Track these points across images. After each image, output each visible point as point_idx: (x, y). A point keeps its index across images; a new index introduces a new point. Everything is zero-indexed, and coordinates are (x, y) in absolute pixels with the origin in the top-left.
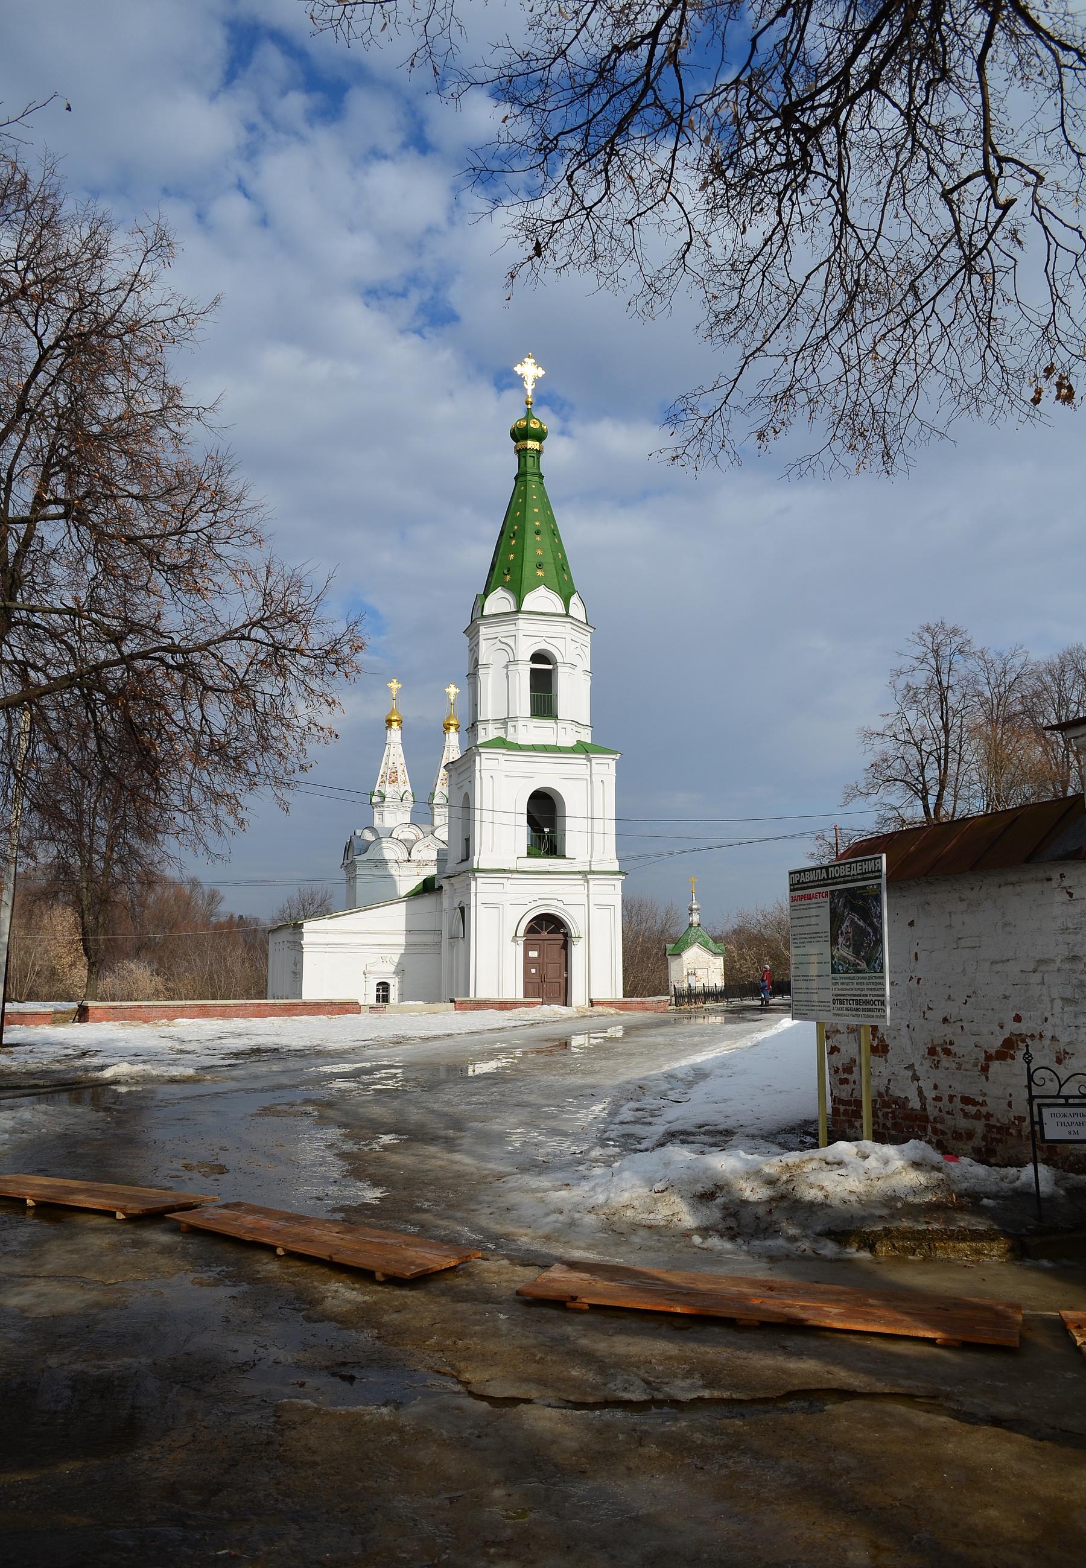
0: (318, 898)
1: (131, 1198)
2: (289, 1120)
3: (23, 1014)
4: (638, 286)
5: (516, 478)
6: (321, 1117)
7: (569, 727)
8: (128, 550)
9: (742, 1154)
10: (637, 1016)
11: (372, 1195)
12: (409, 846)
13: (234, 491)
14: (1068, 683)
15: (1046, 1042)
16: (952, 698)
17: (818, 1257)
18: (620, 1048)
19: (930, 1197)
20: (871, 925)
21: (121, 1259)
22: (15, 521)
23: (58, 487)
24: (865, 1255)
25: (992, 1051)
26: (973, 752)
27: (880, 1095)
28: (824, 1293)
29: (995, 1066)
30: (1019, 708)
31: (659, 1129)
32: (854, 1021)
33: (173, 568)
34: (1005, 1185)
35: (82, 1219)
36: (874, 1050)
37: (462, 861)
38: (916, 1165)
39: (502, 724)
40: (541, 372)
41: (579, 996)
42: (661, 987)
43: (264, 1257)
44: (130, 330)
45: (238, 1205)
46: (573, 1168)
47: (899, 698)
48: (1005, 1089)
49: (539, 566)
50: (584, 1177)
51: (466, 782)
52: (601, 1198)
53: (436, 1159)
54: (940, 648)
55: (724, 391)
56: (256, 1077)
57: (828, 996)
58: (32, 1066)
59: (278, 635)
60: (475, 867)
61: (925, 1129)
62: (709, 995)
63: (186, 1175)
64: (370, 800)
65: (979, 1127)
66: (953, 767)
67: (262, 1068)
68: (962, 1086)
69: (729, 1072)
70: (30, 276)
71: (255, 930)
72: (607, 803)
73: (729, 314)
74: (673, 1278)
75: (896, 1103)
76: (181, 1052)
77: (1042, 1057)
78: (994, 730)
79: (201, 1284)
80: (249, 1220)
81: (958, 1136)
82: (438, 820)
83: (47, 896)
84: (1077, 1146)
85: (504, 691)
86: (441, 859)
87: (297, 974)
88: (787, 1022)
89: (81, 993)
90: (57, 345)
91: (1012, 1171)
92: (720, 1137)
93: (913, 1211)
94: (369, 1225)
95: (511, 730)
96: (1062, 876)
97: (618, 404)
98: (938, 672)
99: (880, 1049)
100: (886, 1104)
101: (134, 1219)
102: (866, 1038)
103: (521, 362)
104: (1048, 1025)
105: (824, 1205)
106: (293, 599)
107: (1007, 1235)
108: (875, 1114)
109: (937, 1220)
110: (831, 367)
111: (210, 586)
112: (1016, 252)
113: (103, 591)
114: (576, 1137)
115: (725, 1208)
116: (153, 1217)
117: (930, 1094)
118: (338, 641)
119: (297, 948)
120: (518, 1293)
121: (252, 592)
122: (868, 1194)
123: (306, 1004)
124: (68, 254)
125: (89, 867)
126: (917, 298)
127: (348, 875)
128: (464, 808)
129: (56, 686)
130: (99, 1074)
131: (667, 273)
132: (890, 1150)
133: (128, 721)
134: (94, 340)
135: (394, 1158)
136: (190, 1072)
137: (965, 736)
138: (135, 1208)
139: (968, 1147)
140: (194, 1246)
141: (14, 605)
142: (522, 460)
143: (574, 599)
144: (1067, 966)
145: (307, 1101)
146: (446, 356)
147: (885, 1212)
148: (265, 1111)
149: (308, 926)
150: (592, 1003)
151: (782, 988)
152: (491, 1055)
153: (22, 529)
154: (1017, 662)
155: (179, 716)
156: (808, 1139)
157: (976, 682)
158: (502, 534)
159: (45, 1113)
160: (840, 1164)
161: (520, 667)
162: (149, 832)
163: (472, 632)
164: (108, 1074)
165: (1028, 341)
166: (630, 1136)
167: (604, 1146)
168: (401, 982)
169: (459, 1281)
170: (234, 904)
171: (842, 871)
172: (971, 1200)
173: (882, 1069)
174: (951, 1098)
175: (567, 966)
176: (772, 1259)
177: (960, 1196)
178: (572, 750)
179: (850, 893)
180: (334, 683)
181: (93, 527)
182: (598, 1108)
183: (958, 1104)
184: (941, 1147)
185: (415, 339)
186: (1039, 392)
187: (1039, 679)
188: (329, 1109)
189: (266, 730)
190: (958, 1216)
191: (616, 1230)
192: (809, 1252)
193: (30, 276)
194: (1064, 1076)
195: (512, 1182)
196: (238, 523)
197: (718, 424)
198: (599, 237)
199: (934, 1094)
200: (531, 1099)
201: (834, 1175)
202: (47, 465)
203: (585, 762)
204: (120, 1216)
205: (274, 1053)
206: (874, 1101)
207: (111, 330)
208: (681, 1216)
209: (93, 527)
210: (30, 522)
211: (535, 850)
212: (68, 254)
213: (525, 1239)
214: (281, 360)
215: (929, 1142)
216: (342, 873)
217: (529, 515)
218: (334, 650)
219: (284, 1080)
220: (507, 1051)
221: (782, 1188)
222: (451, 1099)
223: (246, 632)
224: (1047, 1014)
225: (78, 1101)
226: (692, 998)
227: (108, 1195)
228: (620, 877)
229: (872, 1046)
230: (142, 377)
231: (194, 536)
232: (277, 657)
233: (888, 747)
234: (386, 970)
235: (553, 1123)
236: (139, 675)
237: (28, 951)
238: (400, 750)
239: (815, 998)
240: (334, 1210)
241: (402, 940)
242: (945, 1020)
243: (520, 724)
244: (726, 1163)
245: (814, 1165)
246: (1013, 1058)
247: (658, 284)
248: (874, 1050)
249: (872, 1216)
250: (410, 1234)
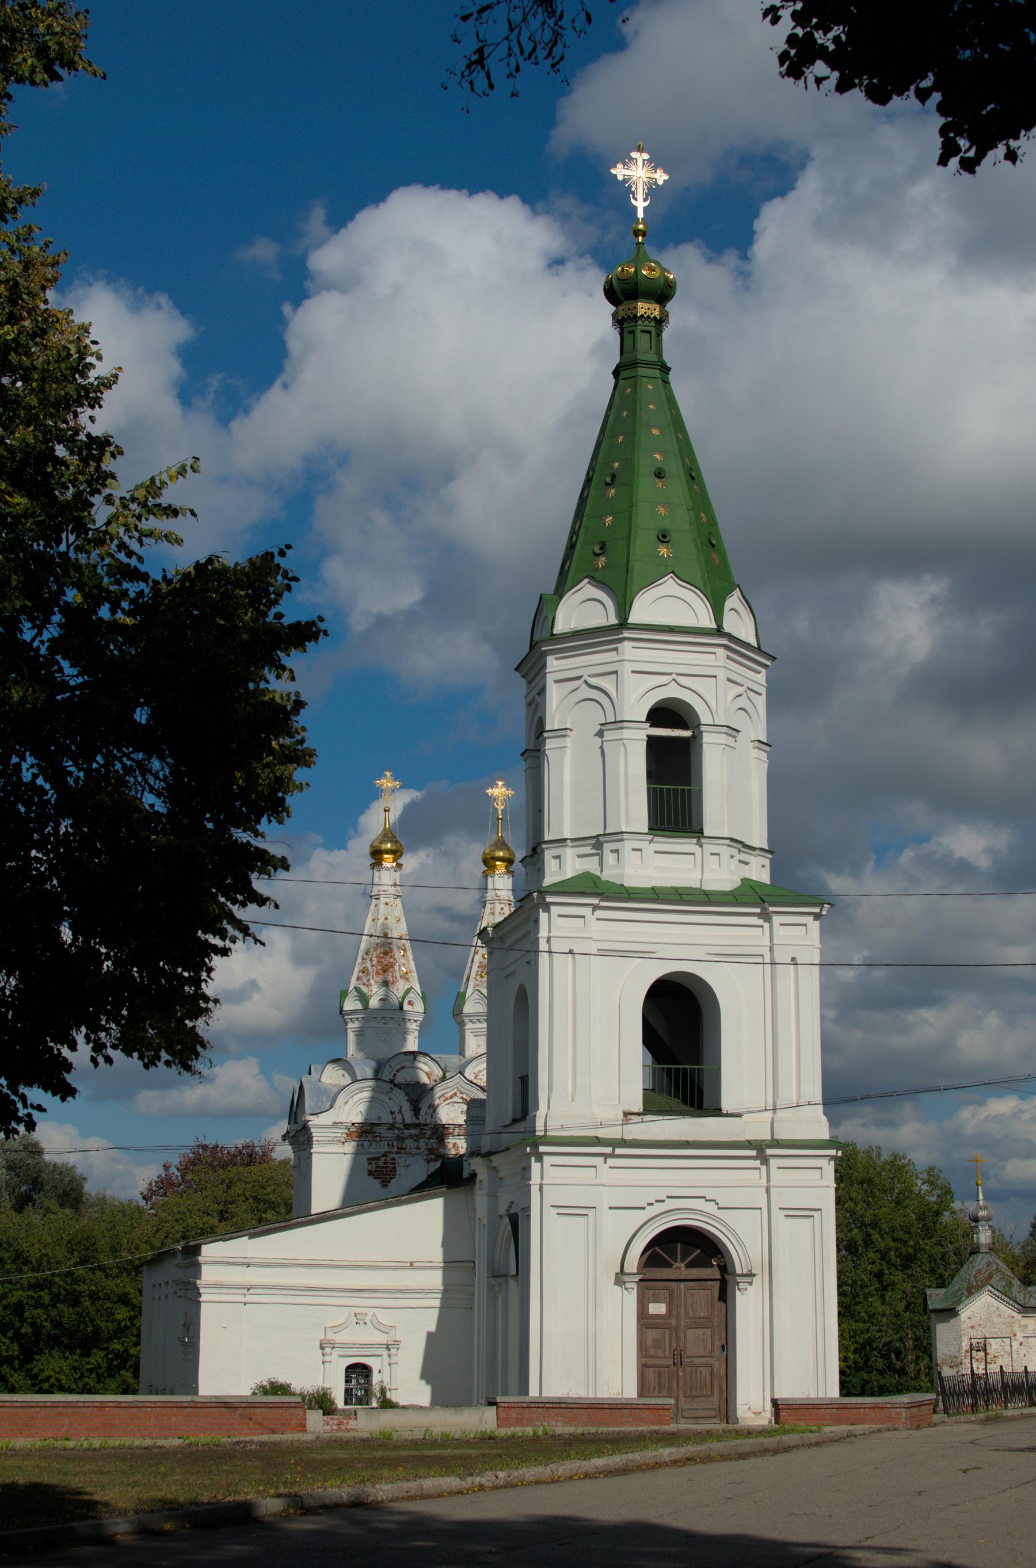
5: (616, 373)
7: (725, 851)
37: (515, 1121)
39: (594, 847)
49: (663, 538)
60: (540, 1133)
72: (803, 998)
95: (610, 858)
103: (627, 161)
119: (189, 1295)
142: (628, 338)
143: (734, 601)
149: (210, 1251)
158: (589, 480)
161: (626, 734)
163: (531, 668)
203: (760, 922)
211: (663, 1099)
228: (833, 1152)
241: (435, 1279)
243: (628, 845)
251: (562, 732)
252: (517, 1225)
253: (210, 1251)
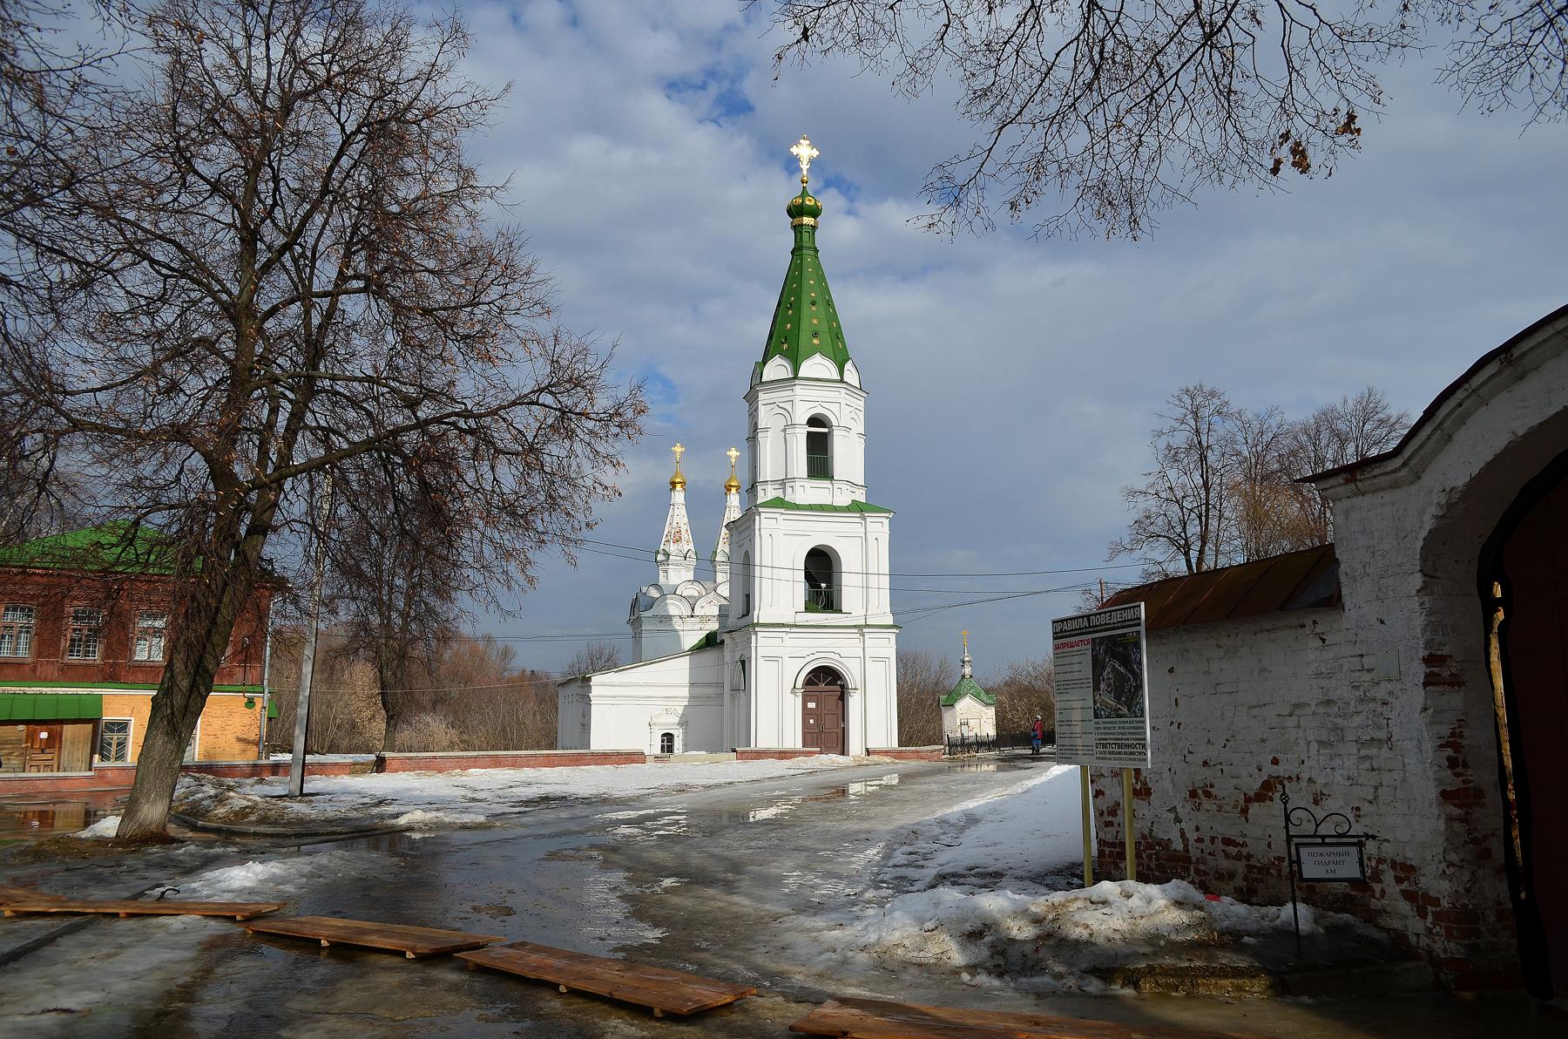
0: (606, 653)
1: (420, 938)
3: (324, 765)
4: (902, 66)
6: (606, 861)
7: (844, 487)
8: (432, 323)
9: (1009, 893)
10: (913, 764)
11: (652, 935)
12: (692, 602)
13: (523, 264)
14: (1324, 442)
15: (1304, 784)
16: (1212, 458)
17: (1084, 994)
18: (895, 795)
20: (1132, 671)
21: (410, 996)
22: (318, 295)
23: (360, 262)
24: (1129, 992)
25: (1251, 794)
26: (1232, 509)
27: (1144, 837)
28: (1089, 1028)
29: (1255, 808)
31: (930, 872)
32: (1116, 765)
33: (465, 337)
34: (1265, 923)
35: (373, 958)
36: (1136, 793)
38: (1179, 904)
40: (815, 153)
41: (855, 746)
42: (936, 738)
43: (547, 995)
44: (427, 116)
45: (523, 944)
46: (847, 908)
48: (1264, 829)
49: (815, 335)
50: (858, 918)
52: (873, 938)
53: (715, 900)
54: (1198, 407)
55: (977, 162)
56: (544, 824)
57: (1091, 740)
58: (330, 814)
59: (567, 401)
61: (1188, 870)
62: (982, 744)
63: (475, 916)
64: (655, 559)
65: (1240, 867)
66: (1213, 524)
67: (549, 815)
69: (1000, 817)
70: (336, 68)
71: (547, 685)
73: (985, 93)
74: (942, 1014)
75: (1159, 844)
76: (474, 800)
77: (1299, 797)
79: (487, 1021)
80: (534, 959)
81: (1220, 876)
82: (720, 577)
83: (348, 652)
84: (1335, 884)
85: (783, 453)
86: (723, 615)
87: (585, 726)
88: (1057, 770)
89: (379, 745)
90: (358, 131)
91: (1273, 910)
92: (990, 878)
93: (1176, 948)
94: (649, 964)
95: (789, 490)
96: (1315, 622)
98: (1197, 432)
99: (1143, 792)
100: (1150, 846)
101: (425, 959)
102: (1129, 780)
103: (797, 143)
105: (1089, 943)
106: (580, 366)
107: (1268, 972)
108: (1138, 855)
109: (1199, 958)
110: (1078, 139)
111: (501, 354)
112: (1255, 31)
114: (851, 880)
115: (993, 946)
116: (441, 956)
117: (1192, 836)
118: (621, 405)
119: (586, 700)
120: (791, 1028)
122: (1132, 932)
123: (593, 754)
124: (371, 48)
125: (387, 625)
126: (1161, 74)
127: (635, 630)
128: (745, 566)
129: (355, 450)
131: (927, 53)
132: (1153, 890)
133: (424, 484)
134: (394, 125)
135: (675, 900)
136: (482, 819)
137: (1225, 493)
138: (424, 948)
139: (1230, 887)
140: (479, 984)
143: (849, 366)
144: (1322, 710)
145: (593, 847)
146: (741, 143)
147: (1148, 950)
148: (553, 856)
149: (596, 679)
150: (868, 752)
151: (1049, 738)
152: (770, 802)
153: (325, 303)
154: (1273, 422)
155: (470, 476)
157: (1234, 442)
159: (341, 858)
160: (1105, 903)
162: (443, 591)
163: (751, 398)
164: (403, 821)
165: (1266, 114)
166: (902, 878)
167: (877, 888)
168: (685, 733)
169: (734, 1017)
170: (528, 659)
171: (1103, 619)
172: (1232, 938)
174: (1213, 839)
175: (844, 716)
176: (1039, 996)
177: (1221, 934)
178: (848, 509)
179: (1109, 645)
181: (392, 300)
182: (872, 852)
183: (1219, 845)
184: (1203, 887)
185: (712, 128)
186: (1278, 162)
187: (1295, 438)
188: (613, 854)
189: (556, 492)
191: (887, 967)
192: (1074, 989)
194: (1319, 817)
195: (788, 922)
196: (527, 295)
197: (973, 193)
198: (862, 22)
199: (1195, 835)
200: (808, 843)
201: (1098, 914)
202: (349, 245)
204: (410, 955)
205: (563, 800)
206: (1138, 844)
207: (409, 116)
208: (950, 954)
209: (392, 300)
210: (333, 295)
211: (813, 606)
212: (371, 48)
213: (799, 977)
214: (586, 148)
215: (1192, 882)
216: (629, 629)
218: (617, 414)
220: (786, 798)
221: (1048, 927)
222: (731, 844)
223: (534, 398)
224: (1304, 757)
225: (376, 848)
226: (966, 746)
227: (399, 935)
229: (1135, 790)
230: (439, 160)
231: (486, 307)
233: (1151, 504)
234: (670, 721)
235: (829, 867)
236: (434, 439)
237: (329, 706)
238: (683, 511)
239: (1079, 742)
240: (616, 950)
241: (685, 692)
242: (1205, 763)
243: (798, 484)
244: (993, 903)
245: (1079, 904)
246: (1271, 799)
247: (919, 64)
248: (1136, 793)
249: (1136, 954)
250: (688, 972)
251: (766, 429)
252: (744, 664)
253: (596, 679)
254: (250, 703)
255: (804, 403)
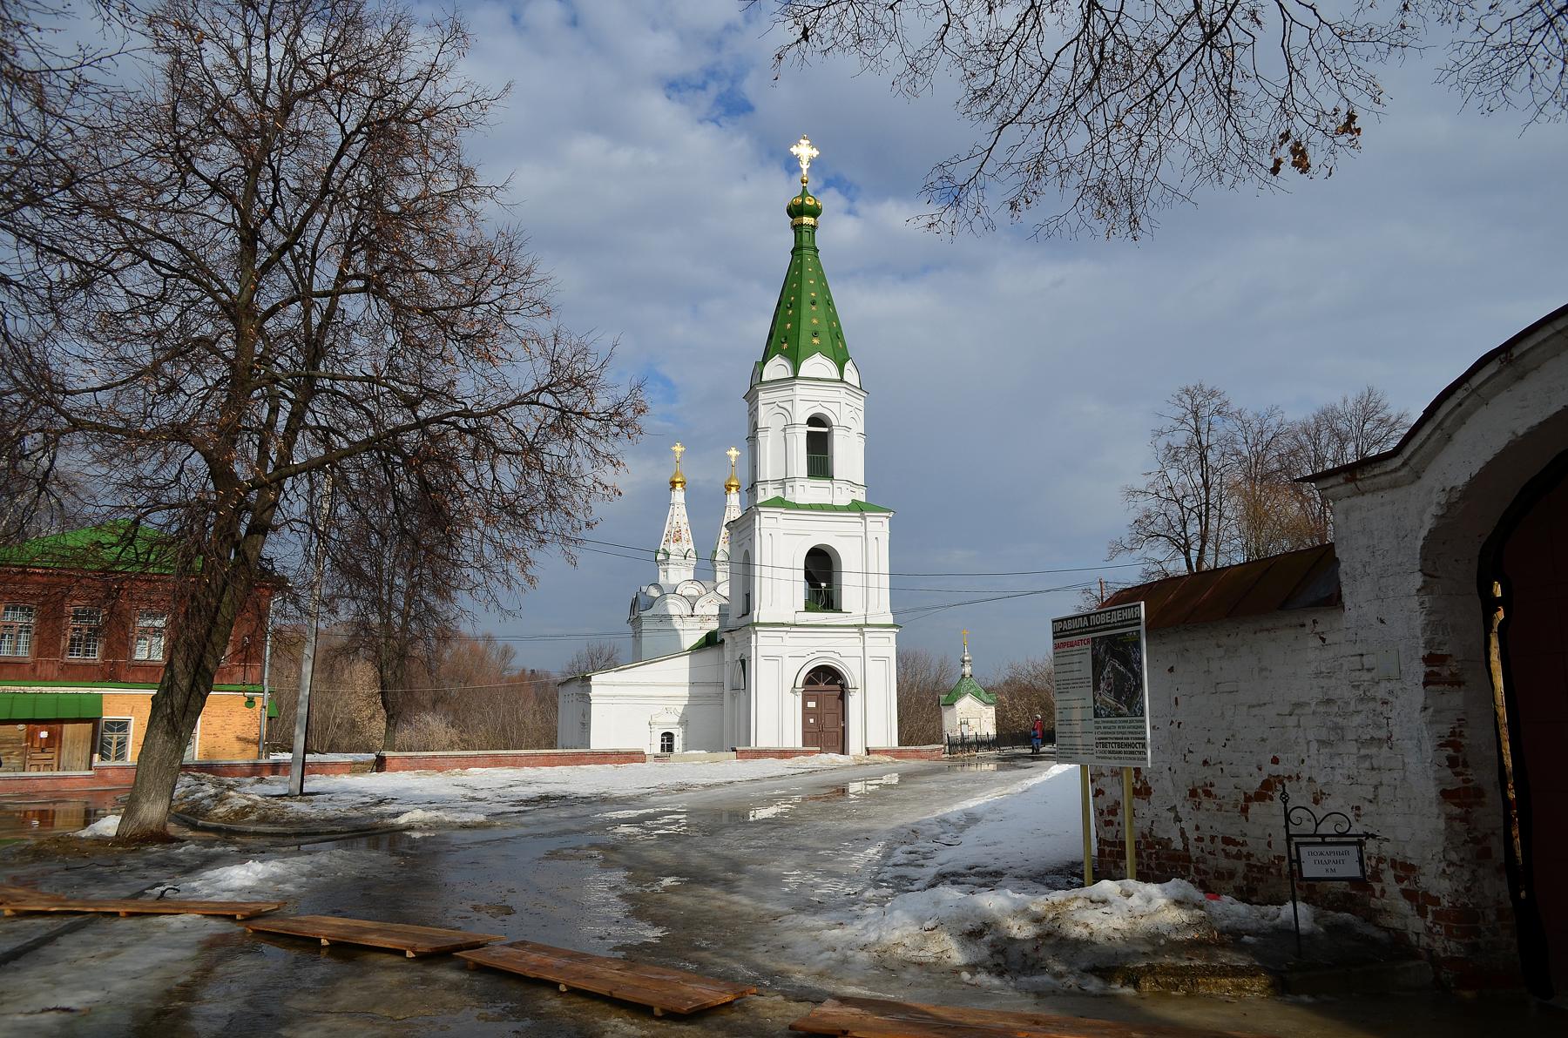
0: (606, 652)
1: (420, 937)
2: (573, 863)
3: (324, 764)
4: (902, 66)
6: (606, 860)
7: (844, 487)
8: (431, 323)
9: (1009, 892)
10: (913, 764)
11: (652, 934)
12: (692, 602)
14: (1324, 442)
15: (1304, 783)
16: (1212, 457)
17: (1084, 993)
18: (895, 794)
19: (1192, 935)
20: (1132, 670)
21: (410, 995)
22: (318, 295)
23: (360, 261)
24: (1129, 991)
26: (1232, 508)
27: (1144, 836)
28: (1089, 1027)
29: (1255, 807)
30: (1276, 466)
31: (931, 871)
32: (1116, 764)
33: (465, 337)
34: (1265, 923)
35: (373, 957)
36: (1136, 792)
38: (1179, 903)
40: (815, 153)
41: (855, 745)
42: (936, 738)
43: (547, 994)
44: (427, 116)
45: (523, 943)
46: (847, 907)
47: (1161, 457)
48: (1264, 828)
49: (815, 334)
50: (858, 917)
51: (746, 541)
52: (873, 937)
53: (715, 899)
54: (1199, 407)
55: (978, 161)
56: (544, 823)
57: (1091, 739)
61: (1188, 869)
62: (981, 743)
63: (475, 916)
64: (655, 558)
65: (1240, 866)
66: (1213, 523)
67: (549, 814)
68: (1222, 827)
69: (1000, 816)
70: (336, 68)
71: (547, 684)
72: (881, 560)
73: (985, 92)
75: (1159, 843)
76: (474, 799)
77: (1299, 796)
78: (1253, 488)
80: (534, 958)
81: (1220, 875)
82: (720, 577)
83: (348, 651)
85: (783, 453)
86: (723, 615)
87: (585, 725)
88: (1057, 769)
89: (379, 744)
90: (358, 130)
91: (1273, 909)
92: (990, 878)
93: (1177, 947)
94: (649, 963)
95: (789, 490)
97: (893, 185)
98: (1198, 432)
99: (1143, 792)
100: (1150, 846)
101: (425, 958)
102: (1129, 780)
103: (797, 143)
104: (1304, 767)
105: (1089, 943)
106: (580, 365)
107: (1268, 971)
108: (1138, 854)
109: (1199, 957)
110: (1078, 139)
111: (501, 354)
112: (1255, 31)
113: (401, 361)
114: (851, 879)
115: (993, 945)
116: (441, 955)
117: (1192, 835)
118: (621, 405)
119: (586, 700)
120: (791, 1027)
121: (542, 359)
122: (1132, 931)
123: (593, 754)
124: (371, 48)
125: (387, 624)
126: (1161, 74)
127: (636, 629)
128: (745, 565)
129: (354, 450)
130: (394, 821)
131: (927, 53)
132: (1153, 889)
134: (394, 125)
135: (675, 899)
136: (482, 818)
137: (1225, 493)
138: (424, 947)
139: (1230, 886)
140: (479, 983)
141: (316, 373)
143: (849, 365)
144: (1322, 709)
145: (593, 846)
146: (741, 143)
147: (1148, 949)
148: (553, 855)
149: (596, 679)
150: (868, 751)
151: (1049, 737)
152: (770, 801)
153: (325, 302)
154: (1273, 422)
155: (470, 476)
156: (1076, 880)
157: (1234, 441)
159: (341, 858)
160: (1105, 902)
162: (443, 590)
163: (751, 397)
164: (402, 820)
165: (1266, 114)
166: (902, 877)
167: (877, 887)
168: (685, 733)
169: (734, 1016)
170: (527, 658)
171: (1103, 619)
172: (1232, 937)
173: (1145, 811)
174: (1213, 838)
175: (844, 715)
176: (1039, 995)
177: (1221, 933)
178: (848, 509)
179: (1109, 644)
180: (618, 445)
181: (392, 300)
182: (872, 852)
183: (1219, 845)
184: (1203, 886)
185: (712, 128)
186: (1278, 162)
187: (1295, 438)
188: (613, 853)
189: (556, 491)
190: (1220, 953)
191: (888, 966)
192: (1075, 988)
193: (336, 68)
194: (1319, 816)
195: (788, 921)
197: (973, 193)
198: (862, 21)
200: (809, 842)
201: (1098, 913)
202: (349, 245)
204: (410, 954)
205: (563, 800)
206: (1138, 843)
207: (409, 116)
208: (950, 953)
209: (392, 300)
210: (333, 295)
211: (813, 605)
212: (371, 48)
213: (799, 976)
214: (587, 148)
215: (1192, 882)
216: (629, 628)
217: (805, 286)
218: (617, 413)
219: (573, 827)
220: (786, 797)
221: (1048, 927)
222: (731, 844)
223: (534, 398)
224: (1304, 756)
225: (376, 847)
226: (965, 746)
227: (400, 935)
230: (439, 160)
231: (486, 307)
232: (564, 422)
233: (1152, 504)
235: (829, 866)
236: (434, 439)
237: (329, 705)
239: (1079, 741)
240: (616, 949)
241: (685, 691)
242: (1205, 763)
243: (798, 484)
244: (993, 902)
245: (1079, 903)
246: (1271, 799)
247: (919, 64)
248: (1136, 792)
250: (688, 971)
251: (766, 429)
254: (250, 702)
255: (805, 402)
